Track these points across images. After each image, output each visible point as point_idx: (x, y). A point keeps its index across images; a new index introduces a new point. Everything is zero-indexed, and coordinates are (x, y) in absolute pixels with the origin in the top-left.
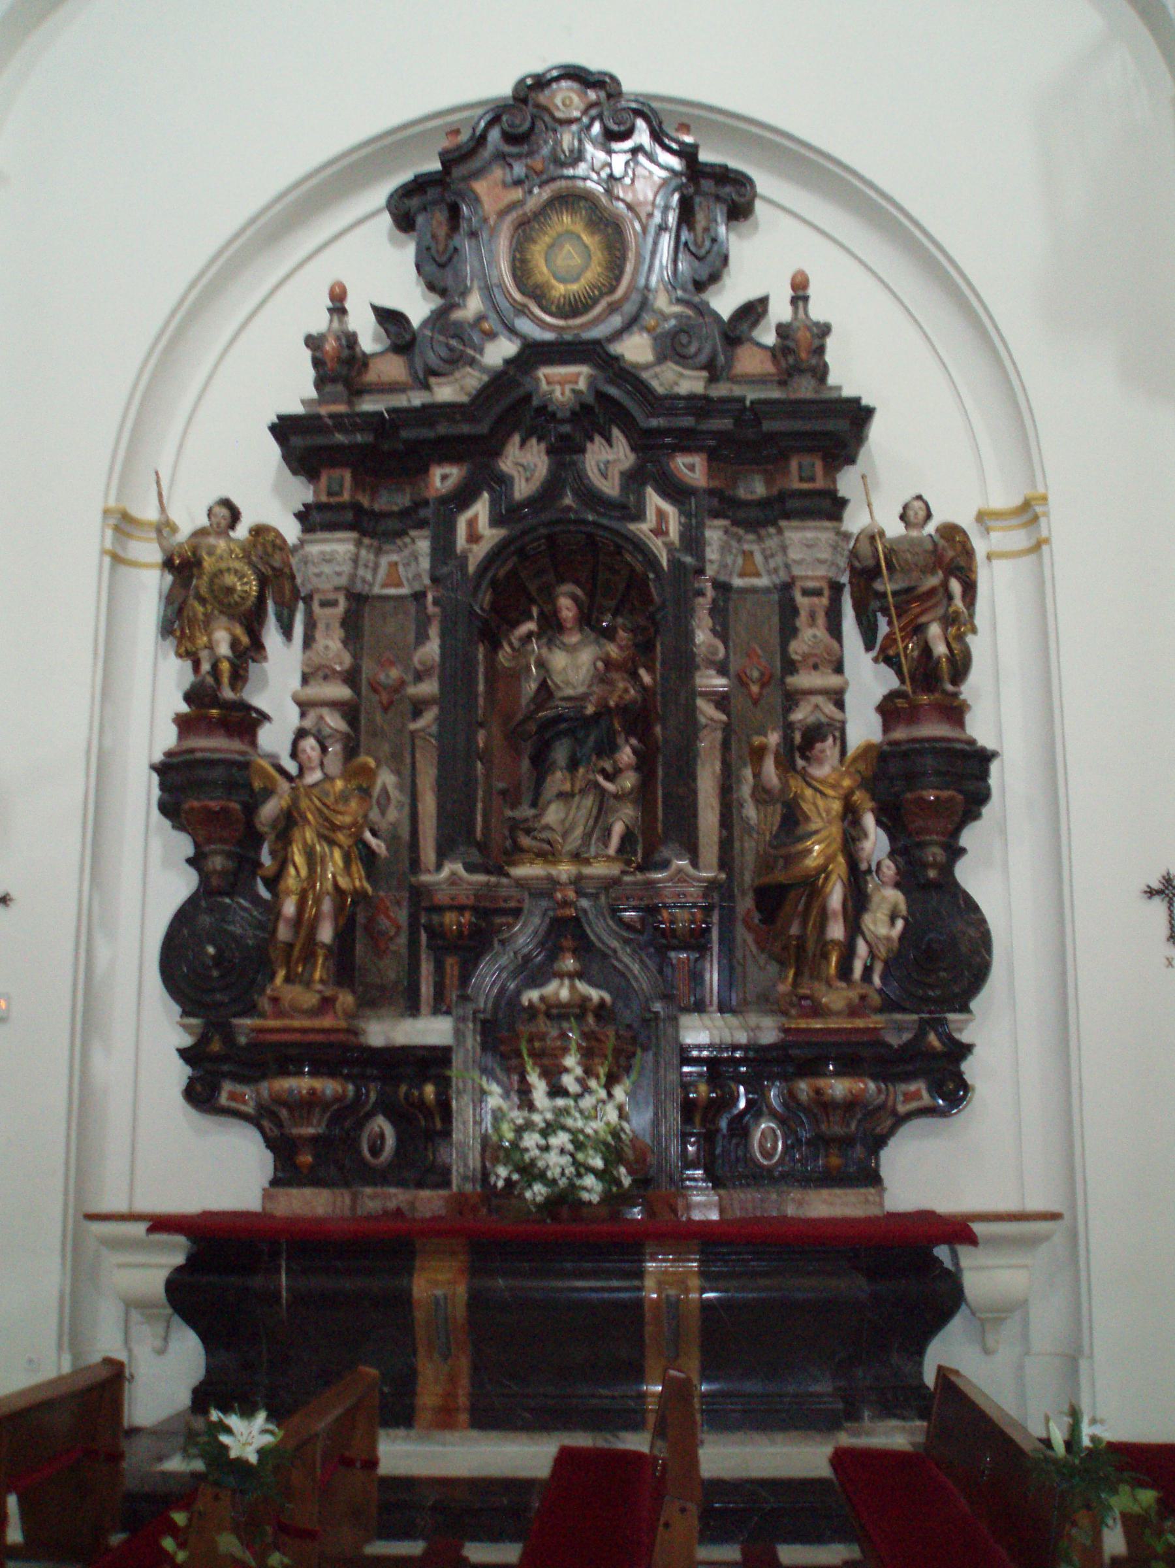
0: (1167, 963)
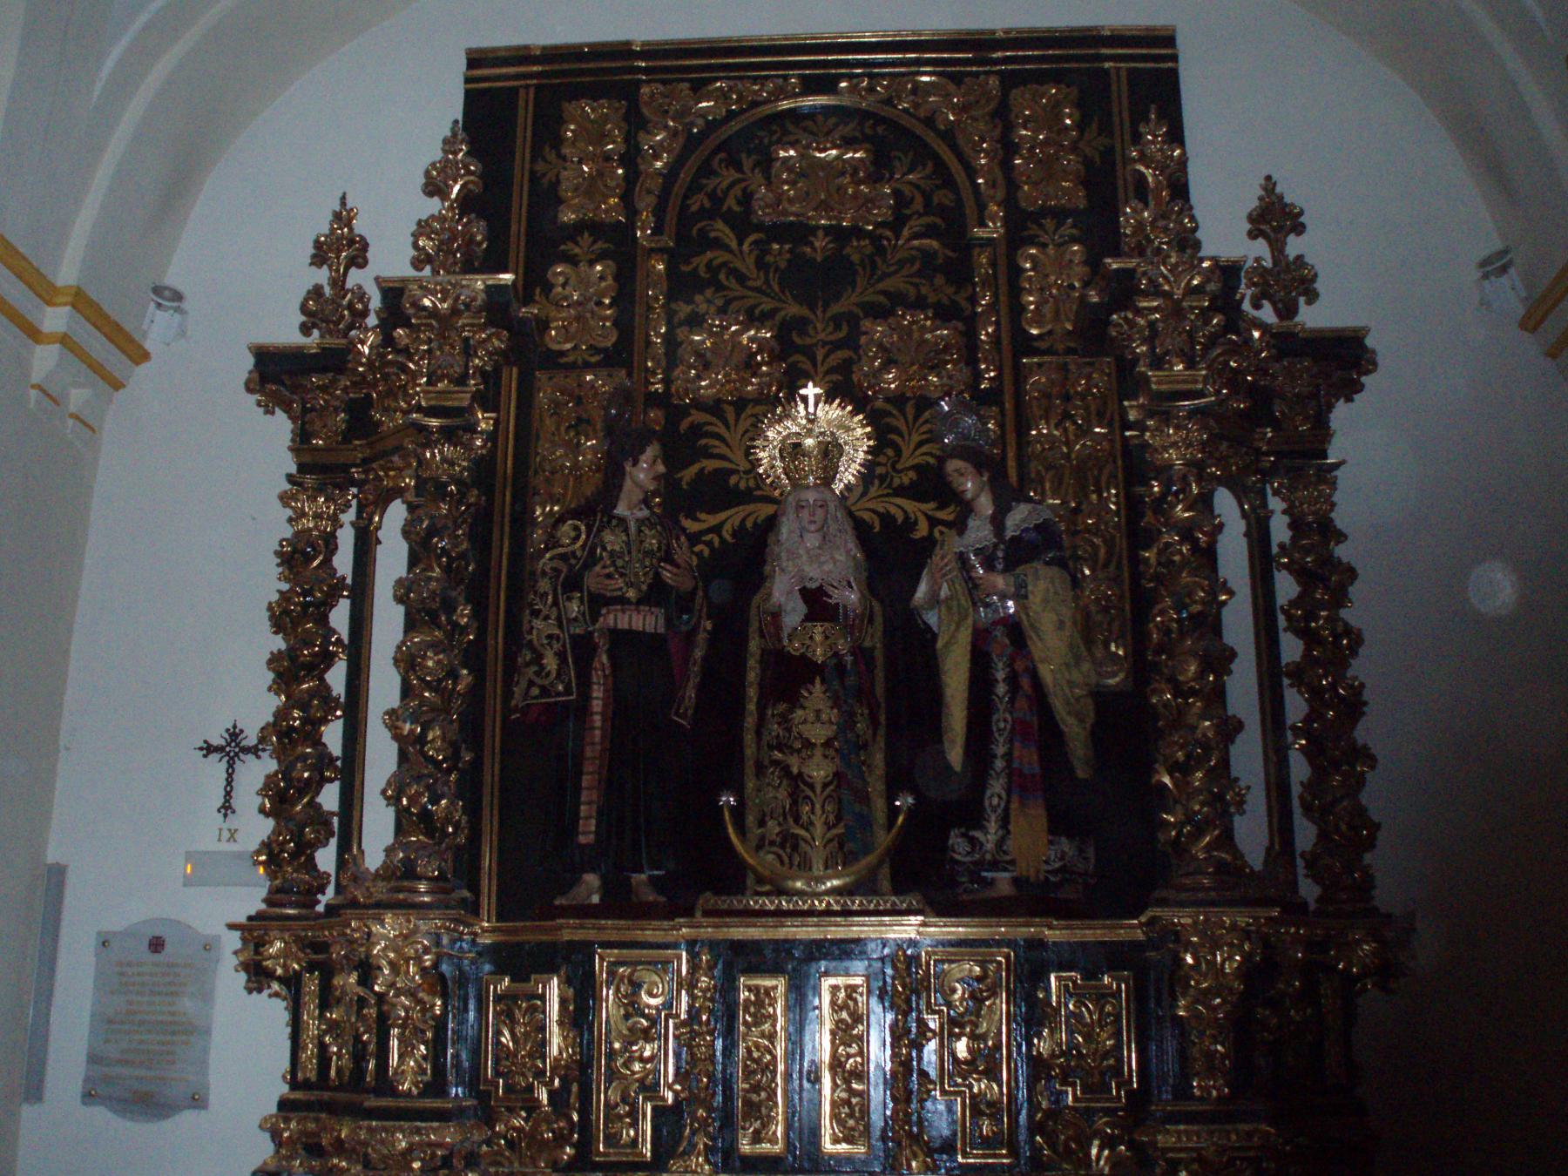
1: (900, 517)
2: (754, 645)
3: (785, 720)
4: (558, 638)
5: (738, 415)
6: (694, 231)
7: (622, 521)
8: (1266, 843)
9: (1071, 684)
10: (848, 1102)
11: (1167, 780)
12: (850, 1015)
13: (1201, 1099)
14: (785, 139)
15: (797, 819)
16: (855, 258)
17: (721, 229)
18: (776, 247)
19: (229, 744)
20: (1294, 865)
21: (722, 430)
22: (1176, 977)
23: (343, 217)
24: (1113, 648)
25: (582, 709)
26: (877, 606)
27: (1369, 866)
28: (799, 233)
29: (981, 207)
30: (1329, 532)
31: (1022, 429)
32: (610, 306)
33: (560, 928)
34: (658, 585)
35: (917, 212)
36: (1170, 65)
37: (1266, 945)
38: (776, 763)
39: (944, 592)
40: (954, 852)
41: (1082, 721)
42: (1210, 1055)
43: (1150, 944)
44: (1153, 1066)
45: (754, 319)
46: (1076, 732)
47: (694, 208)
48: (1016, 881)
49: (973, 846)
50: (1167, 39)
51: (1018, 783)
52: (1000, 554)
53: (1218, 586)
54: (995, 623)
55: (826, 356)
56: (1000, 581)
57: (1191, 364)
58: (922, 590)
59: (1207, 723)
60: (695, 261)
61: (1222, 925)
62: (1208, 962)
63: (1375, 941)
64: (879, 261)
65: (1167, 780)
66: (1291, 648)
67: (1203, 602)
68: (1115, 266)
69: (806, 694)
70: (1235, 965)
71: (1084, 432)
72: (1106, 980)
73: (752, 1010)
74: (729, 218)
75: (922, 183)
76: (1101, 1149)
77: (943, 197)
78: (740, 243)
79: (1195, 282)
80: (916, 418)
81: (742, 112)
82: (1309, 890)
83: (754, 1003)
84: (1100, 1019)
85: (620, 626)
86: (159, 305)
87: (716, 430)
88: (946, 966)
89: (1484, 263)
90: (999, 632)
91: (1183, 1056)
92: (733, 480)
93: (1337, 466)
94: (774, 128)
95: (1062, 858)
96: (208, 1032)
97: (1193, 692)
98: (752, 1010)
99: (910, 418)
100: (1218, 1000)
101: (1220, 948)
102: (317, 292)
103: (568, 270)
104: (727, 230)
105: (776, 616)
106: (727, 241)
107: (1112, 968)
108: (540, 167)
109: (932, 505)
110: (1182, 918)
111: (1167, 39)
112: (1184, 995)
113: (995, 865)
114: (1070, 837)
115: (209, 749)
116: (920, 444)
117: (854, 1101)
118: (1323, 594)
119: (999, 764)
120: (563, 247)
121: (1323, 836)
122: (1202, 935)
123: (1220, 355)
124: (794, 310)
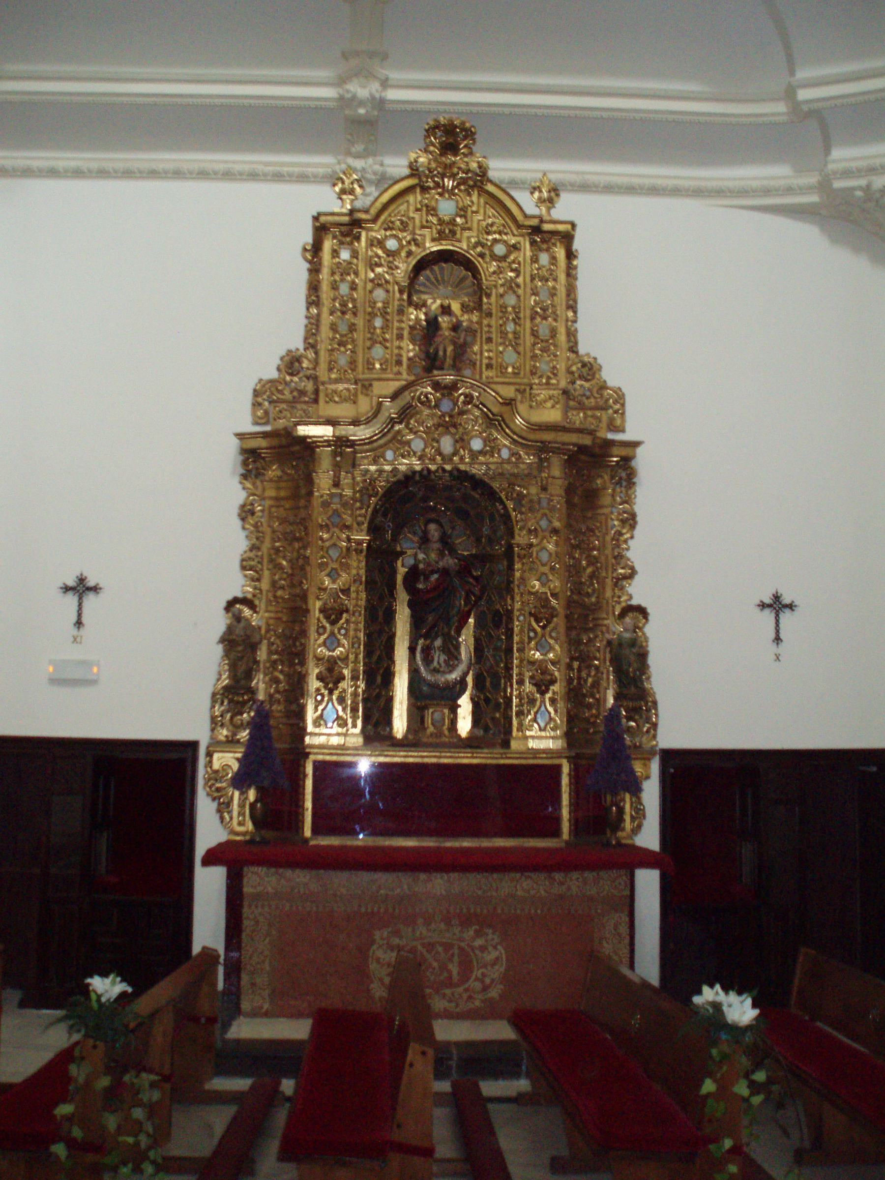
0: (775, 658)
115: (67, 589)
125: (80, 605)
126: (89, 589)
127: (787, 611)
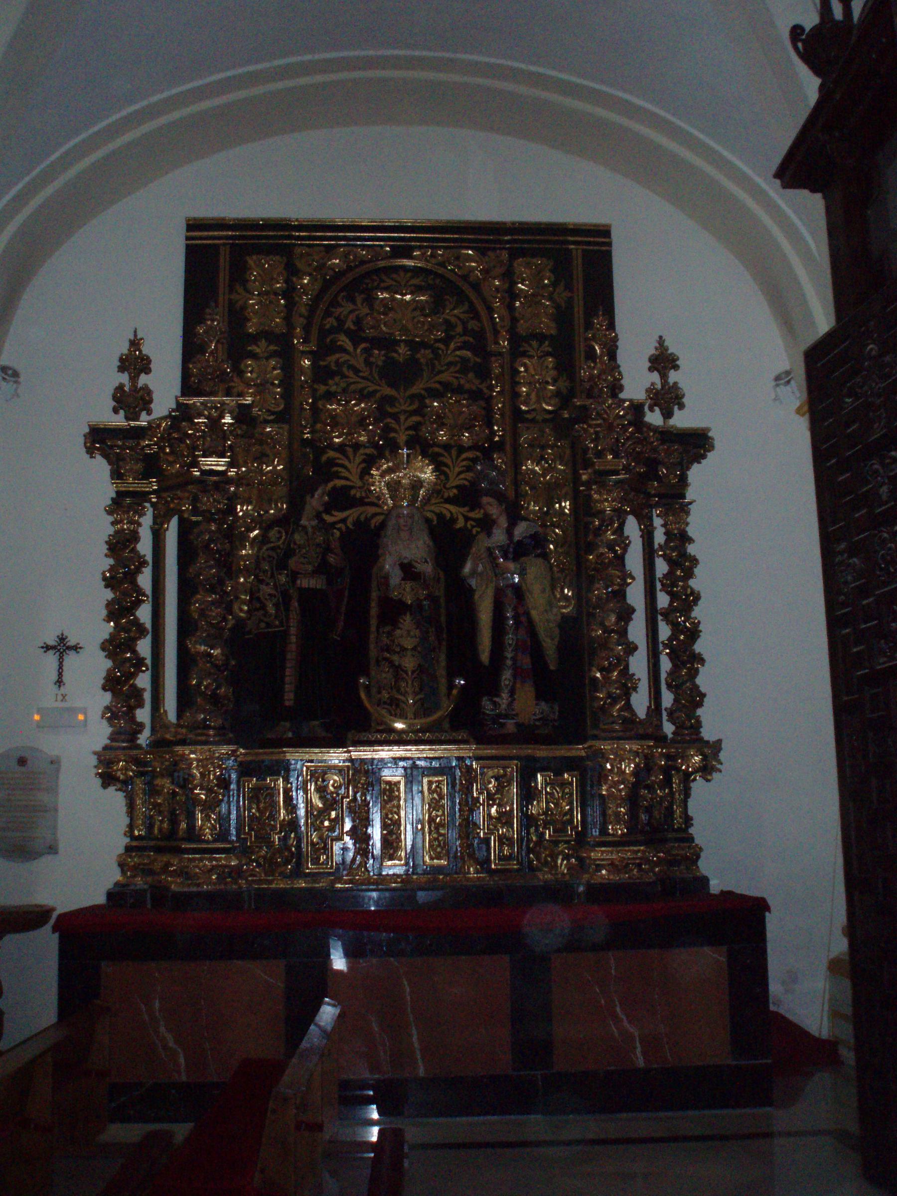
1: (448, 515)
2: (374, 595)
3: (389, 634)
4: (275, 596)
5: (355, 454)
6: (328, 340)
7: (304, 527)
8: (648, 704)
9: (548, 621)
10: (436, 839)
11: (598, 675)
12: (438, 795)
13: (613, 835)
14: (382, 285)
15: (398, 691)
16: (422, 361)
17: (344, 340)
18: (376, 352)
19: (59, 645)
20: (661, 714)
21: (346, 463)
22: (602, 776)
23: (135, 343)
24: (566, 591)
25: (286, 633)
26: (442, 574)
27: (699, 716)
28: (387, 343)
29: (496, 333)
30: (684, 538)
31: (516, 465)
32: (279, 386)
33: (285, 752)
34: (324, 563)
35: (459, 334)
36: (607, 248)
37: (646, 757)
38: (385, 659)
39: (480, 568)
40: (485, 708)
41: (552, 639)
42: (617, 814)
43: (588, 757)
44: (589, 819)
45: (363, 396)
46: (550, 646)
47: (328, 326)
48: (518, 725)
49: (496, 707)
50: (604, 232)
51: (517, 673)
52: (511, 550)
53: (626, 575)
54: (508, 586)
55: (406, 419)
56: (511, 566)
57: (616, 456)
58: (467, 569)
59: (620, 647)
60: (329, 359)
61: (625, 750)
62: (618, 768)
63: (701, 755)
64: (436, 362)
65: (598, 675)
66: (663, 600)
67: (619, 584)
68: (578, 403)
69: (402, 621)
70: (631, 769)
71: (551, 469)
72: (566, 776)
73: (387, 793)
74: (349, 333)
75: (462, 316)
76: (563, 860)
77: (472, 325)
78: (355, 349)
79: (621, 413)
80: (457, 458)
81: (356, 266)
82: (669, 728)
83: (389, 790)
84: (562, 796)
85: (303, 586)
86: (4, 379)
87: (343, 462)
88: (485, 770)
89: (777, 378)
90: (509, 592)
91: (604, 814)
92: (353, 492)
93: (690, 503)
94: (375, 277)
95: (542, 713)
96: (56, 810)
97: (613, 631)
98: (387, 793)
99: (454, 457)
100: (622, 786)
101: (624, 761)
102: (120, 388)
103: (254, 364)
104: (347, 341)
105: (386, 578)
106: (348, 348)
107: (569, 770)
108: (234, 297)
109: (466, 509)
110: (605, 746)
111: (604, 232)
112: (605, 784)
113: (506, 716)
114: (547, 701)
115: (47, 648)
116: (460, 473)
117: (441, 838)
118: (681, 573)
119: (509, 663)
120: (249, 348)
121: (676, 701)
122: (616, 754)
123: (630, 445)
124: (388, 391)
125: (61, 667)
126: (69, 648)
127: (72, 653)
